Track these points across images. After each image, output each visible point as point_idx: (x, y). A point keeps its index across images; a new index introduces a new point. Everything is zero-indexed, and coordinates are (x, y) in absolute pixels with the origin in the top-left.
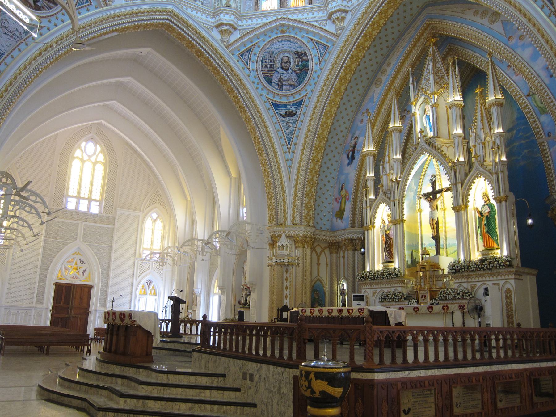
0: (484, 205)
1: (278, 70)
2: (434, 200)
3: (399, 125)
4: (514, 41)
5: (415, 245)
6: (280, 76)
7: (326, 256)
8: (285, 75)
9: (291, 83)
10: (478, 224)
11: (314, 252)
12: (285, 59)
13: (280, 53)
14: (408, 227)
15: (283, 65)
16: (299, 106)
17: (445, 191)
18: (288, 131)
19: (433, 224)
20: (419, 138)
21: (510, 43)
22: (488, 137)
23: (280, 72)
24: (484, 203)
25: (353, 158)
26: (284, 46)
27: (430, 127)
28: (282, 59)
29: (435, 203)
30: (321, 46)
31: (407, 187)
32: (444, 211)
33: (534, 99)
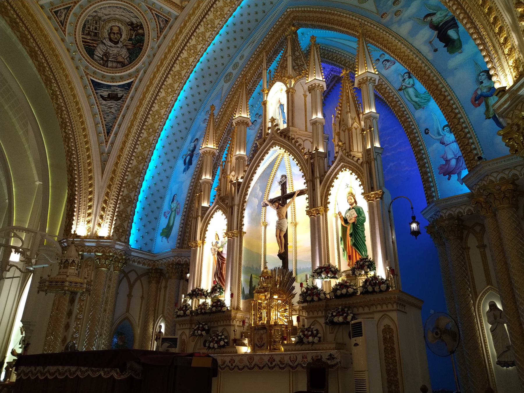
0: (349, 209)
1: (104, 41)
2: (283, 206)
3: (246, 116)
4: (388, 18)
5: (256, 268)
6: (106, 48)
7: (142, 286)
8: (113, 49)
9: (120, 59)
10: (340, 235)
11: (125, 281)
12: (116, 30)
13: (109, 20)
14: (248, 243)
15: (112, 36)
16: (127, 89)
17: (298, 195)
18: (109, 119)
19: (280, 237)
20: (269, 128)
21: (384, 21)
22: (356, 123)
23: (106, 43)
24: (349, 207)
25: (190, 163)
26: (115, 13)
27: (284, 118)
28: (111, 29)
29: (284, 209)
30: (161, 19)
31: (250, 190)
32: (296, 225)
33: (408, 92)
